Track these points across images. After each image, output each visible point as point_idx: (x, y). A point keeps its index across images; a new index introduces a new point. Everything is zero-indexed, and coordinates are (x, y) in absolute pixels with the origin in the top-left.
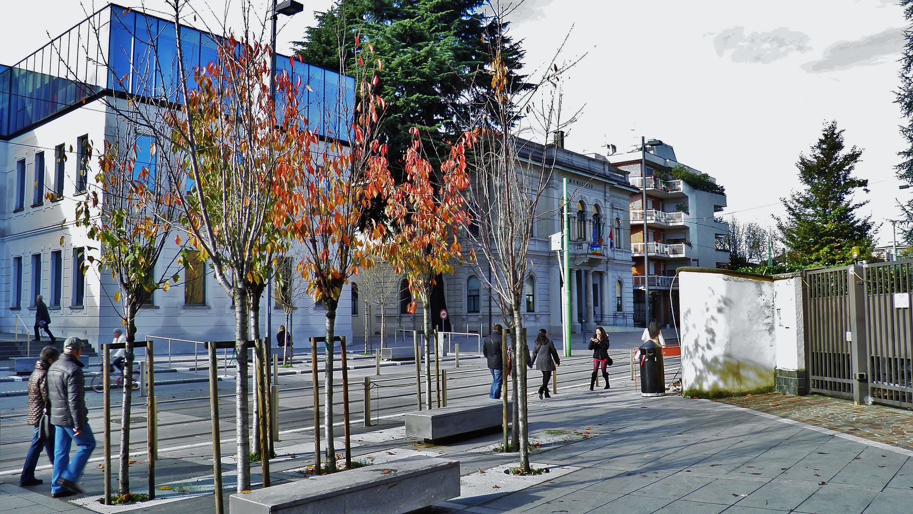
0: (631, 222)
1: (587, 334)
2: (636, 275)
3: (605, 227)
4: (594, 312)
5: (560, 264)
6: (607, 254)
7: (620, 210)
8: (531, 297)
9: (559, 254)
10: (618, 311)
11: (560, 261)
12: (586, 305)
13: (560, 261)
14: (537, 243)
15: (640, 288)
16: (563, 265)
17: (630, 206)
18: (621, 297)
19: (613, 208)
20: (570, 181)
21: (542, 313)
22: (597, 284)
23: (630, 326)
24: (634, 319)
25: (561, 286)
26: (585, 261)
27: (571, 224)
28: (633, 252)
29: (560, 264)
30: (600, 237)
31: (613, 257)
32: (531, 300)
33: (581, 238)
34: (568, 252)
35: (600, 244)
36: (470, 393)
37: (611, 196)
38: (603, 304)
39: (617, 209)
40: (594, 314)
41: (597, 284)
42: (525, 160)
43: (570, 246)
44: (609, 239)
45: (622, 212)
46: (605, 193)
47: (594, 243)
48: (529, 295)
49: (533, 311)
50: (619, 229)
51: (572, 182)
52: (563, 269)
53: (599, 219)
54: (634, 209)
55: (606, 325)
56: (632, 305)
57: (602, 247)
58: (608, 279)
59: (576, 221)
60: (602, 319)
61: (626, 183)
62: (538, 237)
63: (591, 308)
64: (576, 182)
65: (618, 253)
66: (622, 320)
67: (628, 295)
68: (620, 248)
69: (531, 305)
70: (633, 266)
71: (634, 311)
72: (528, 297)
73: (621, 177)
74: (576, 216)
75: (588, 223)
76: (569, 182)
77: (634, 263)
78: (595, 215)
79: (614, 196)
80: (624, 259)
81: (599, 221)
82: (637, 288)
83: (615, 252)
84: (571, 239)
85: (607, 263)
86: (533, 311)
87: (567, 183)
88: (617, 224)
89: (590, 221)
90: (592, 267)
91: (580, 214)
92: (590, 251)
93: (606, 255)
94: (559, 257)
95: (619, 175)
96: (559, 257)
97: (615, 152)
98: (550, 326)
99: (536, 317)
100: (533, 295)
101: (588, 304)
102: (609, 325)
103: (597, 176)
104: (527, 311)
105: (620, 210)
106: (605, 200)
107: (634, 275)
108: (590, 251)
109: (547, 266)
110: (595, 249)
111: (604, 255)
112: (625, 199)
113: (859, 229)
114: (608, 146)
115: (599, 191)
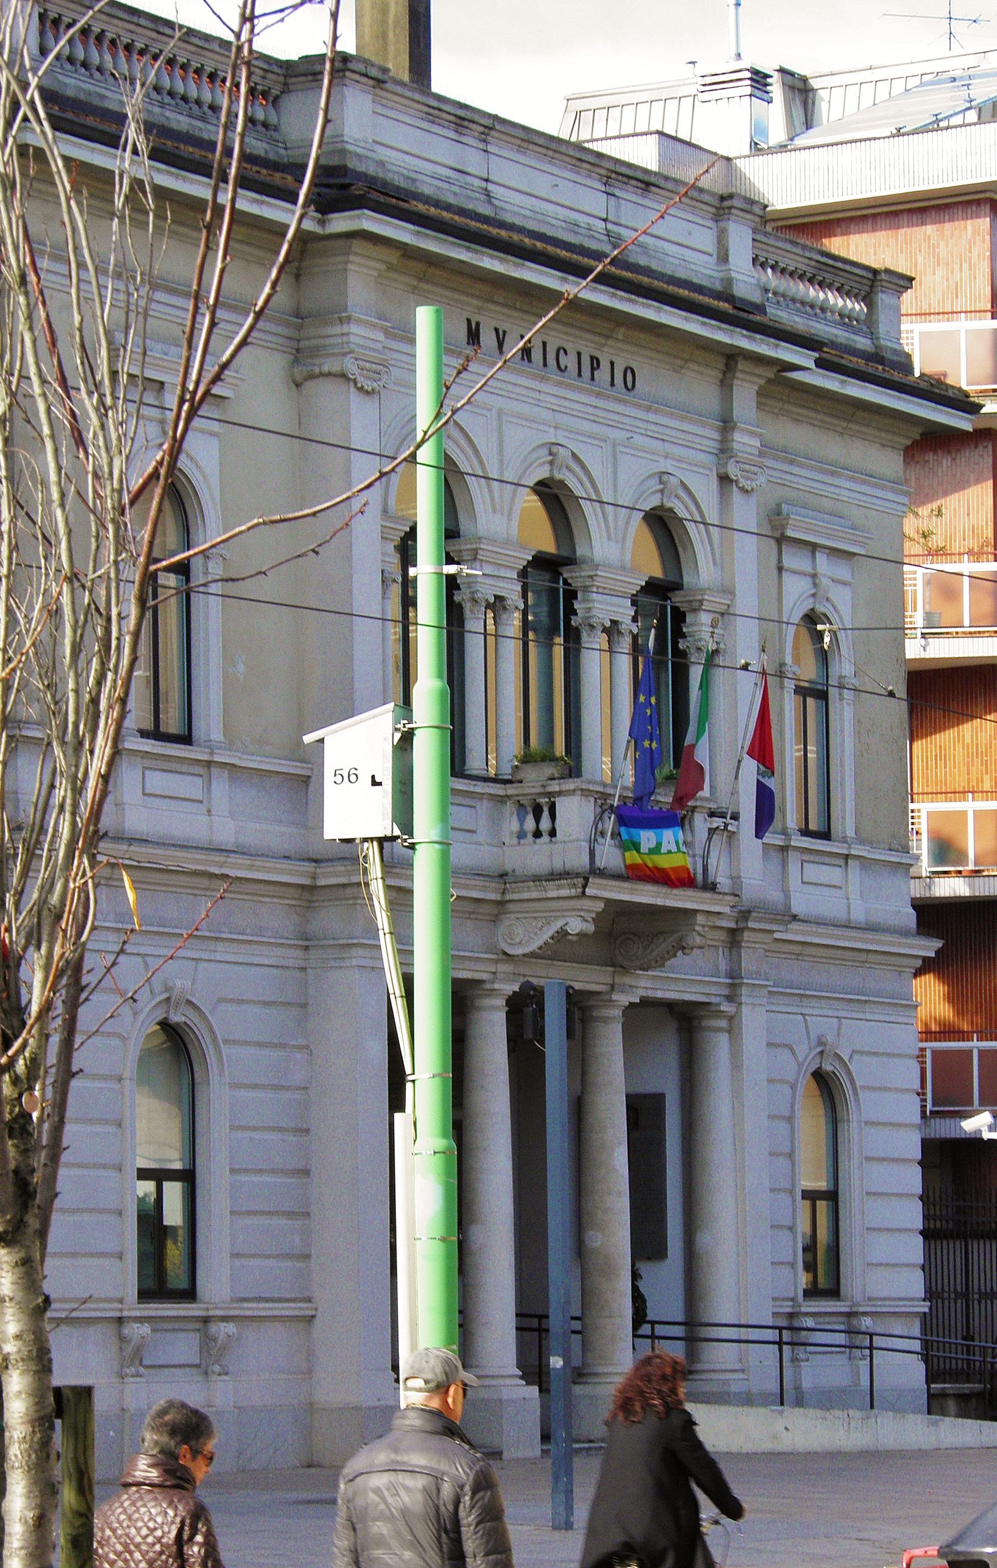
0: (914, 649)
1: (577, 1461)
2: (947, 1032)
3: (720, 677)
4: (639, 1300)
5: (386, 944)
6: (736, 879)
7: (834, 552)
8: (173, 1192)
9: (375, 869)
10: (812, 1292)
11: (382, 920)
12: (580, 1250)
13: (382, 920)
14: (221, 786)
15: (969, 1125)
16: (405, 953)
17: (910, 525)
18: (832, 1196)
19: (781, 540)
20: (473, 336)
21: (251, 1309)
22: (658, 1100)
23: (897, 1408)
24: (926, 1357)
25: (397, 1102)
26: (576, 926)
27: (474, 647)
28: (925, 866)
29: (386, 944)
30: (682, 753)
31: (774, 896)
32: (173, 1215)
33: (547, 757)
34: (445, 857)
35: (680, 800)
36: (823, 1357)
37: (767, 449)
38: (704, 1239)
39: (813, 547)
40: (639, 1317)
41: (658, 1100)
42: (198, 187)
43: (463, 816)
44: (750, 767)
45: (842, 570)
46: (727, 425)
47: (642, 795)
48: (158, 1176)
49: (189, 1294)
50: (822, 696)
51: (488, 339)
52: (408, 982)
53: (679, 616)
54: (940, 553)
55: (720, 1398)
56: (914, 1249)
57: (701, 823)
58: (736, 1064)
59: (514, 622)
60: (692, 1355)
61: (876, 357)
62: (230, 744)
63: (609, 1272)
64: (569, 361)
65: (814, 872)
66: (839, 1360)
67: (878, 1177)
68: (826, 835)
69: (175, 1253)
70: (926, 967)
71: (931, 1294)
72: (147, 1187)
73: (845, 318)
74: (512, 591)
75: (594, 643)
76: (91, 195)
77: (929, 947)
78: (542, 563)
79: (787, 455)
80: (858, 915)
81: (678, 634)
82: (943, 1129)
83: (794, 860)
84: (475, 762)
85: (734, 938)
86: (189, 1294)
87: (444, 347)
88: (808, 648)
89: (612, 630)
90: (618, 965)
91: (540, 580)
92: (609, 856)
93: (723, 882)
94: (377, 888)
95: (834, 300)
96: (377, 888)
97: (808, 125)
98: (311, 1407)
99: (207, 1341)
100: (188, 1177)
101: (595, 1240)
102: (747, 1400)
103: (603, 279)
104: (145, 1295)
105: (834, 552)
106: (724, 479)
107: (928, 1035)
108: (609, 856)
109: (294, 957)
110: (647, 838)
111: (710, 887)
112: (868, 477)
113: (23, 1265)
114: (759, 80)
115: (685, 412)
